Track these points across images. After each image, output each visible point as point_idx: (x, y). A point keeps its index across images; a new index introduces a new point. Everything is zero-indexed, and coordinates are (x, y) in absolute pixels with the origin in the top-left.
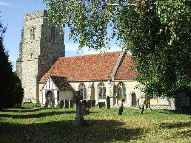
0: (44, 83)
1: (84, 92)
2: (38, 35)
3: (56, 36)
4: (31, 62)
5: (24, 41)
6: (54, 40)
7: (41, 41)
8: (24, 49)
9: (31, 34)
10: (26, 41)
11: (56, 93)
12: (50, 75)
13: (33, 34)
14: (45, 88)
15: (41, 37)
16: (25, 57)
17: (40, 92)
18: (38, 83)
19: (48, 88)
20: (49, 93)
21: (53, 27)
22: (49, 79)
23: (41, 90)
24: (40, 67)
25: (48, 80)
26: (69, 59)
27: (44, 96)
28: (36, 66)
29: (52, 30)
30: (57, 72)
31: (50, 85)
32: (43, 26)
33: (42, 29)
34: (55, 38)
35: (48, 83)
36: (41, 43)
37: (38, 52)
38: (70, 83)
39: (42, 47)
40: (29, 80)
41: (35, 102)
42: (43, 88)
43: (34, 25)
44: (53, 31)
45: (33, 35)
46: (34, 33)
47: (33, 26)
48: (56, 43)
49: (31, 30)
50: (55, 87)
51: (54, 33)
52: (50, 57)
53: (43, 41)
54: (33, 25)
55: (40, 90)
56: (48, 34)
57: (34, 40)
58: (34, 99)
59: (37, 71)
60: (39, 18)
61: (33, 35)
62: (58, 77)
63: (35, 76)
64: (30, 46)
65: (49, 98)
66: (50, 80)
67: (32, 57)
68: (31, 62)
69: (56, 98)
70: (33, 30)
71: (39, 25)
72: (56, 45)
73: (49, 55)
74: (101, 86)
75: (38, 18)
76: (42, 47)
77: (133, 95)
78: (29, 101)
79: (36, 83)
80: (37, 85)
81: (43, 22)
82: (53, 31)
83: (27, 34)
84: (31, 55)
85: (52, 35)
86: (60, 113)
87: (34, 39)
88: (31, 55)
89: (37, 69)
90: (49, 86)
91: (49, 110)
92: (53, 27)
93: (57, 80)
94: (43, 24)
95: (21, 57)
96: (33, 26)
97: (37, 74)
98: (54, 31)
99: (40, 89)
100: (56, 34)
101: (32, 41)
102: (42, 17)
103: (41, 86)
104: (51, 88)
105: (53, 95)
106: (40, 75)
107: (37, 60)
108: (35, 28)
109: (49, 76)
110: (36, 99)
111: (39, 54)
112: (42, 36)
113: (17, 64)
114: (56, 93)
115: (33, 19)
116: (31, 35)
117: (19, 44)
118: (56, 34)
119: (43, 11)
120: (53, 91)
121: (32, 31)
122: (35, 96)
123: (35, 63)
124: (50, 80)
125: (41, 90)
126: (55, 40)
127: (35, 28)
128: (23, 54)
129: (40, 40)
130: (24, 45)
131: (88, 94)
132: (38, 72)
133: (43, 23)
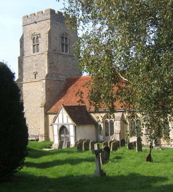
0: (56, 113)
1: (110, 126)
2: (44, 46)
3: (68, 46)
4: (35, 84)
5: (25, 54)
6: (66, 52)
7: (48, 54)
8: (25, 66)
9: (34, 44)
10: (26, 54)
12: (63, 105)
13: (36, 44)
14: (56, 122)
15: (47, 49)
16: (27, 77)
17: (50, 127)
18: (46, 114)
20: (63, 130)
21: (65, 33)
22: (61, 110)
23: (51, 125)
24: (48, 91)
25: (61, 112)
26: (89, 79)
27: (56, 133)
28: (43, 90)
29: (62, 38)
30: (72, 98)
31: (64, 118)
32: (50, 33)
33: (49, 38)
34: (68, 49)
35: (60, 115)
36: (48, 57)
37: (45, 70)
38: (92, 114)
39: (50, 63)
40: (33, 109)
41: (42, 139)
42: (54, 122)
43: (37, 32)
44: (65, 45)
45: (36, 47)
46: (38, 43)
47: (35, 34)
48: (69, 56)
49: (34, 39)
50: (70, 121)
51: (66, 41)
52: (62, 77)
53: (51, 54)
54: (36, 31)
55: (50, 125)
56: (57, 44)
57: (38, 53)
58: (42, 136)
59: (45, 98)
60: (43, 21)
61: (36, 47)
62: (74, 106)
63: (42, 104)
64: (33, 61)
65: (62, 135)
67: (37, 78)
68: (35, 84)
69: (72, 136)
70: (36, 39)
71: (45, 32)
72: (70, 59)
73: (59, 74)
74: (108, 118)
75: (42, 22)
76: (50, 63)
78: (35, 139)
79: (43, 114)
80: (45, 116)
81: (50, 27)
82: (65, 45)
83: (29, 45)
84: (36, 74)
85: (63, 44)
86: (80, 161)
87: (38, 51)
88: (36, 74)
89: (44, 94)
90: (63, 119)
91: (66, 154)
92: (65, 33)
93: (71, 111)
94: (50, 31)
95: (20, 77)
96: (35, 34)
97: (44, 101)
98: (66, 38)
99: (50, 124)
100: (68, 43)
101: (35, 54)
102: (48, 21)
103: (51, 117)
104: (65, 122)
105: (67, 132)
106: (49, 102)
107: (44, 81)
108: (39, 36)
109: (62, 106)
110: (45, 136)
111: (47, 72)
112: (50, 47)
113: (23, 28)
114: (71, 129)
115: (36, 23)
116: (34, 46)
117: (18, 58)
119: (49, 12)
120: (67, 126)
121: (35, 39)
122: (42, 132)
123: (41, 86)
125: (51, 125)
126: (68, 51)
127: (39, 36)
128: (24, 73)
129: (47, 53)
130: (25, 59)
131: (116, 129)
132: (46, 98)
133: (49, 29)
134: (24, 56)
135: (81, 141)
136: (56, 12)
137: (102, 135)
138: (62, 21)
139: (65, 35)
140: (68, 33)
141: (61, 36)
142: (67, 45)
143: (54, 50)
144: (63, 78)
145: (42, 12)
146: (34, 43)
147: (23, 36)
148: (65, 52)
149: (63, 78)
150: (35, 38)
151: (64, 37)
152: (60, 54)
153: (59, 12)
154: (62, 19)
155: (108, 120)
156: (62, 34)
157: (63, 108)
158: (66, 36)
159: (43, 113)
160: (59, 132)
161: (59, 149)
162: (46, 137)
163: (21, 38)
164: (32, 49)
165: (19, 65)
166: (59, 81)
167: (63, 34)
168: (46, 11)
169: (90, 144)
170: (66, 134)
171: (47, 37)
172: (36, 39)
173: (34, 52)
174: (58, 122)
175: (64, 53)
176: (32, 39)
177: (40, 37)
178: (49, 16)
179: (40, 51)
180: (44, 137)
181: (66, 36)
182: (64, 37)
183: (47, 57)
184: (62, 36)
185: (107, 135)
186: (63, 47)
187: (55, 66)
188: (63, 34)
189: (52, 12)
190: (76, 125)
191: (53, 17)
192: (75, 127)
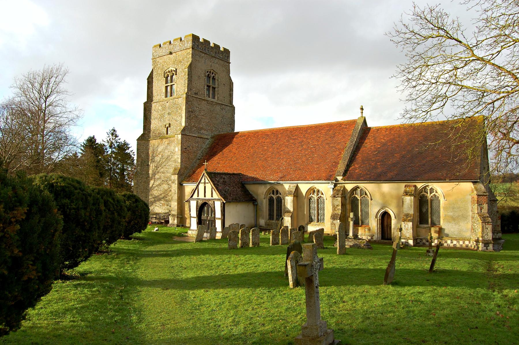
3: (216, 89)
6: (214, 98)
10: (155, 98)
11: (218, 206)
14: (195, 196)
19: (201, 196)
29: (209, 77)
33: (188, 75)
34: (216, 93)
35: (201, 187)
36: (186, 103)
42: (192, 196)
44: (211, 88)
45: (169, 92)
50: (216, 195)
52: (205, 132)
56: (201, 84)
61: (169, 92)
63: (175, 169)
66: (207, 181)
67: (169, 132)
72: (218, 108)
73: (202, 129)
77: (385, 218)
82: (211, 88)
83: (159, 85)
98: (214, 78)
100: (216, 86)
104: (208, 196)
109: (204, 172)
111: (183, 124)
113: (153, 62)
118: (216, 86)
119: (191, 38)
120: (211, 203)
121: (169, 78)
124: (207, 181)
126: (216, 97)
127: (174, 72)
134: (153, 102)
135: (278, 219)
136: (201, 40)
137: (263, 218)
138: (209, 53)
139: (213, 74)
140: (216, 71)
141: (207, 75)
142: (214, 88)
143: (196, 94)
144: (208, 135)
145: (181, 39)
146: (167, 83)
147: (152, 72)
148: (212, 98)
149: (207, 135)
150: (169, 76)
151: (210, 77)
152: (204, 100)
153: (204, 40)
154: (208, 51)
155: (275, 197)
156: (207, 72)
157: (206, 174)
158: (214, 75)
159: (175, 184)
160: (299, 127)
161: (445, 234)
162: (179, 219)
163: (149, 77)
164: (164, 91)
165: (144, 113)
166: (201, 138)
167: (210, 73)
168: (186, 37)
169: (251, 233)
170: (273, 219)
171: (187, 74)
172: (169, 77)
173: (166, 96)
174: (198, 196)
175: (210, 99)
176: (164, 77)
177: (176, 74)
178: (190, 44)
179: (175, 95)
180: (176, 219)
181: (214, 75)
182: (210, 77)
183: (185, 101)
184: (208, 75)
185: (271, 217)
186: (208, 90)
187: (197, 117)
188: (210, 73)
189: (195, 38)
190: (225, 202)
191: (196, 46)
192: (224, 204)
